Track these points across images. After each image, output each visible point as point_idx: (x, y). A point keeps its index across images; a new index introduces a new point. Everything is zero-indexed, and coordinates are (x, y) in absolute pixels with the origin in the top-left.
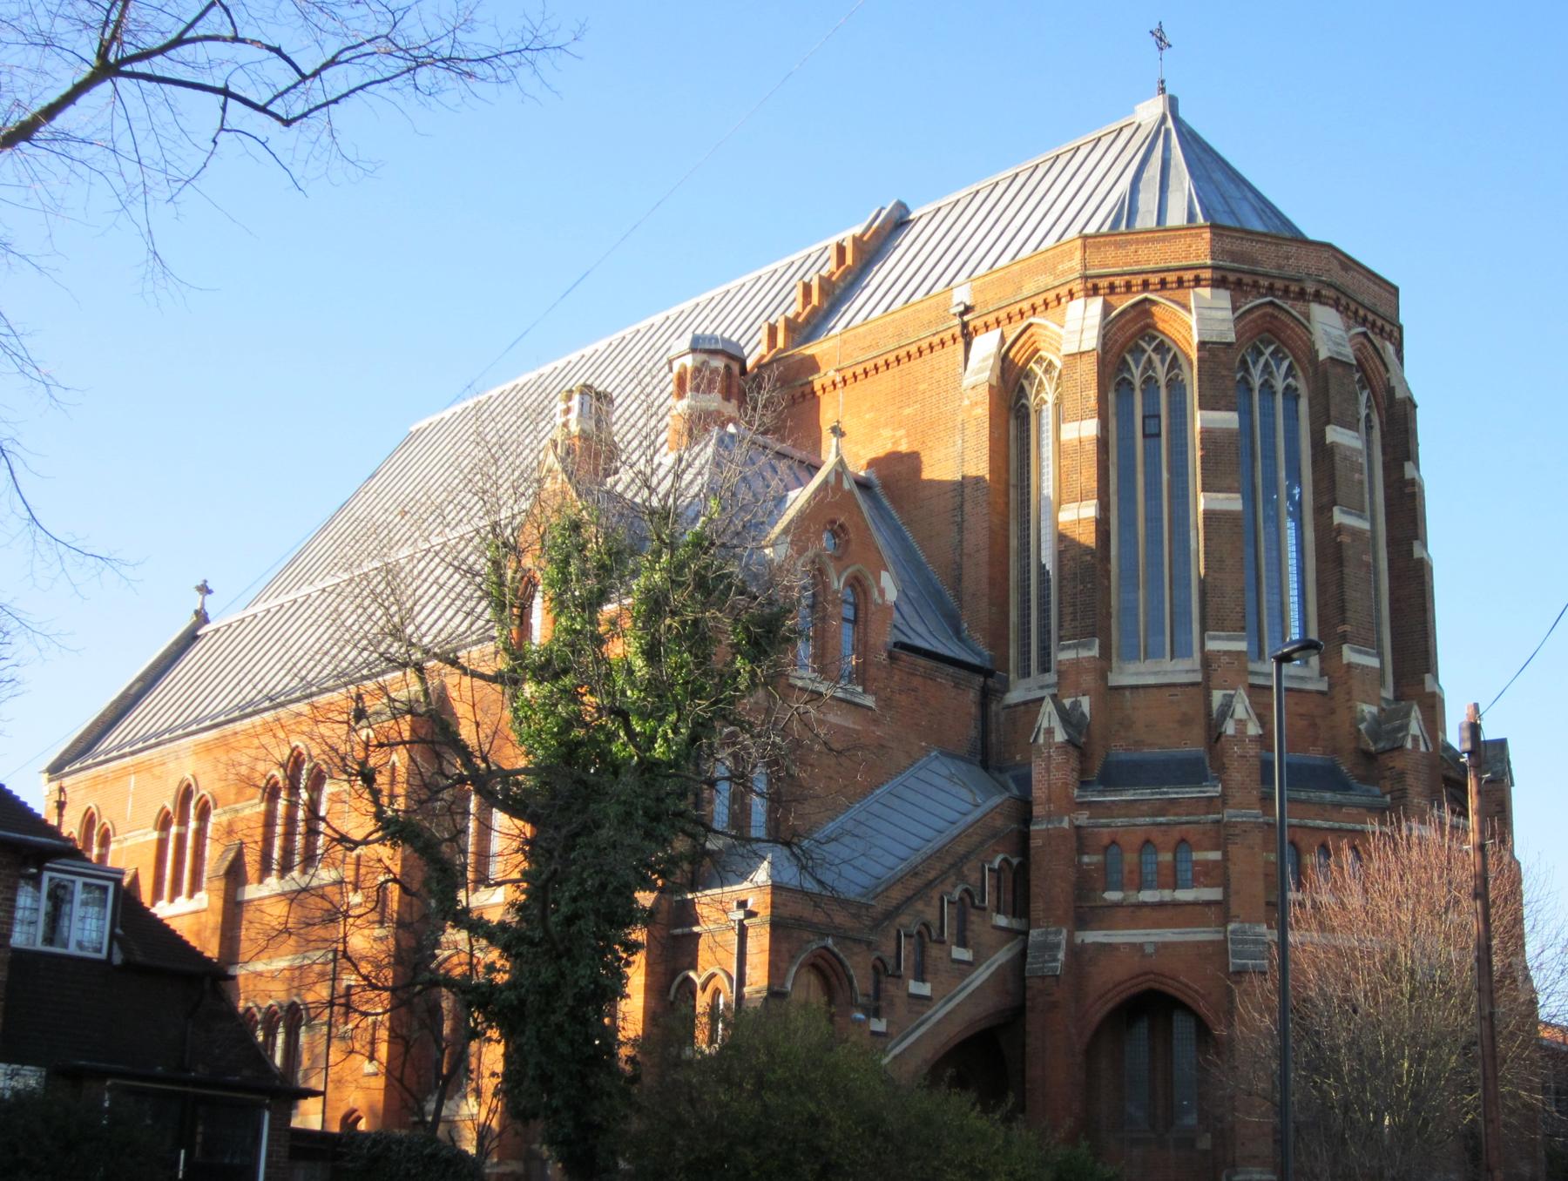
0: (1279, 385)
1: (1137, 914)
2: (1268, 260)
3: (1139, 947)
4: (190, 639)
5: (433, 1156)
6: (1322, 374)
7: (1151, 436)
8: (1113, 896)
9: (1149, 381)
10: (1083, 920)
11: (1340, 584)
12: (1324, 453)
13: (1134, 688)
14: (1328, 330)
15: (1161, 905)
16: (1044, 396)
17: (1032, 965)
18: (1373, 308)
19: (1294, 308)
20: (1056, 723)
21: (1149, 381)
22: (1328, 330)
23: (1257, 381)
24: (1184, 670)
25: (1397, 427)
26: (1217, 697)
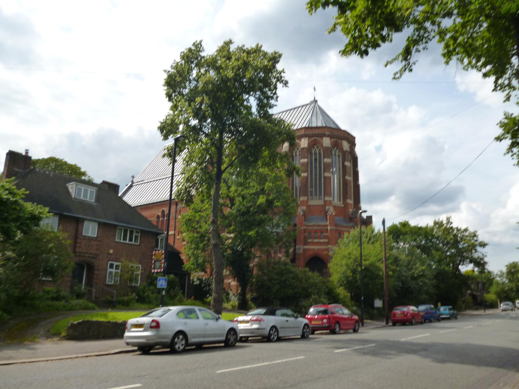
0: (337, 154)
1: (314, 244)
2: (336, 133)
3: (314, 249)
4: (131, 186)
5: (422, 40)
6: (344, 153)
7: (316, 162)
8: (310, 240)
9: (315, 153)
10: (306, 243)
11: (347, 189)
12: (344, 167)
13: (313, 206)
14: (346, 145)
15: (318, 243)
16: (173, 229)
17: (297, 251)
18: (351, 140)
19: (339, 141)
20: (301, 211)
21: (315, 153)
22: (346, 145)
23: (333, 153)
24: (320, 202)
25: (355, 160)
26: (327, 208)
